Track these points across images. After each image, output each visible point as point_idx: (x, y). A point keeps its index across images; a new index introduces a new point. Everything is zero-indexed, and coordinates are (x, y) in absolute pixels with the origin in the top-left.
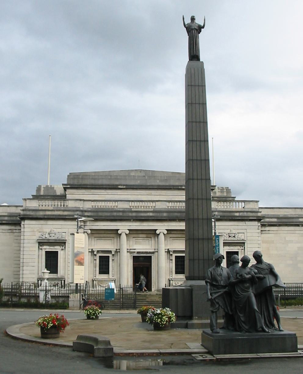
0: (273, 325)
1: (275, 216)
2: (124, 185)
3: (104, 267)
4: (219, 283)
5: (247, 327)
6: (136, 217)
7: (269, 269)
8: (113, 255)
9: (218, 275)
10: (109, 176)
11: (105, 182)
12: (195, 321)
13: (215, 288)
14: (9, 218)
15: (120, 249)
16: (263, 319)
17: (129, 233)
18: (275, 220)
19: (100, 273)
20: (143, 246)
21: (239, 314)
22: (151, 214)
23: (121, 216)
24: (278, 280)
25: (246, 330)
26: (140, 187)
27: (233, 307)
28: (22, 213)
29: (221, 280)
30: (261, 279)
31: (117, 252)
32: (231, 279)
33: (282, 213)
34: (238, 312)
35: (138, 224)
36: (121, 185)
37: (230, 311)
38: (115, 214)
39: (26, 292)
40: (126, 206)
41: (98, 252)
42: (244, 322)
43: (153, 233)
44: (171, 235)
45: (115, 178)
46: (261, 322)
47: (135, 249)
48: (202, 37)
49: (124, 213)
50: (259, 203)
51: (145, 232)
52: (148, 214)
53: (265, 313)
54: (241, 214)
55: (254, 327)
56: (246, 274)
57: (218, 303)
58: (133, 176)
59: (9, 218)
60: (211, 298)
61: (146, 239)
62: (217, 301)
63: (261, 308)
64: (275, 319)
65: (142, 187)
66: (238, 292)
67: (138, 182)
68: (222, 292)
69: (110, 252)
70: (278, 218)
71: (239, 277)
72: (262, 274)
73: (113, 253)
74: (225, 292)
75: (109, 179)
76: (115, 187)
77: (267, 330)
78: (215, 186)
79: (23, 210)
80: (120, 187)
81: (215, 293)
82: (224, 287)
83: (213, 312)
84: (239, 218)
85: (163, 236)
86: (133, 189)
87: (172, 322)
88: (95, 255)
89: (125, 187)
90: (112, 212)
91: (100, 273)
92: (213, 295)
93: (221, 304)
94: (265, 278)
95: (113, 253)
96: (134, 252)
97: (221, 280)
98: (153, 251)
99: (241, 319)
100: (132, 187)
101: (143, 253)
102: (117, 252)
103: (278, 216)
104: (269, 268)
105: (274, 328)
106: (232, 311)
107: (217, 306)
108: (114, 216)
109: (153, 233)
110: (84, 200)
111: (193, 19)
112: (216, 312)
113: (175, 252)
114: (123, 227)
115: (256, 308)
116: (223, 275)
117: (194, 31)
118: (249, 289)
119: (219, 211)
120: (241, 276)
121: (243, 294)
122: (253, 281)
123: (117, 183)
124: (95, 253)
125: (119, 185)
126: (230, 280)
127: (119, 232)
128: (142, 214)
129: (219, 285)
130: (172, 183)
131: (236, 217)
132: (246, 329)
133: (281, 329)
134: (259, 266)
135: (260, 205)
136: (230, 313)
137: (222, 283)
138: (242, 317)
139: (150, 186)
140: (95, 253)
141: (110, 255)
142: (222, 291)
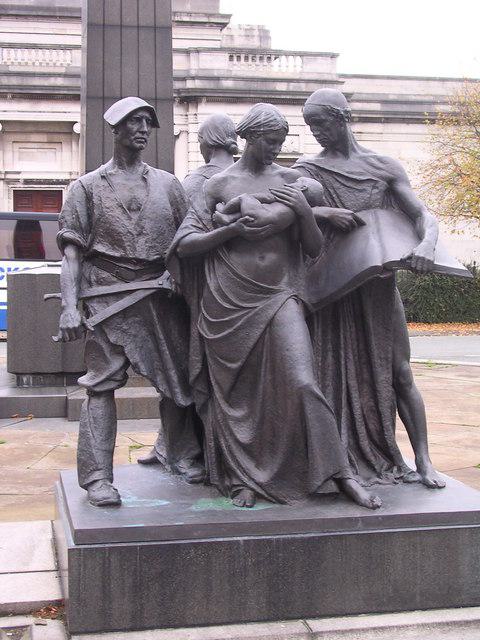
0: (392, 457)
1: (376, 98)
4: (124, 249)
5: (262, 476)
6: (20, 87)
7: (382, 185)
13: (105, 275)
16: (344, 431)
18: (377, 107)
21: (225, 407)
22: (60, 82)
24: (427, 237)
25: (259, 490)
26: (34, 13)
29: (135, 233)
30: (344, 231)
33: (393, 90)
35: (25, 106)
37: (178, 390)
46: (332, 442)
47: (19, 173)
50: (338, 59)
51: (47, 129)
52: (52, 82)
53: (355, 395)
54: (292, 87)
57: (118, 350)
60: (83, 325)
61: (46, 146)
62: (112, 339)
63: (338, 375)
64: (399, 422)
66: (215, 294)
68: (141, 295)
70: (384, 102)
71: (226, 218)
77: (364, 495)
78: (229, 16)
81: (105, 298)
84: (288, 97)
86: (17, 16)
92: (94, 306)
93: (134, 358)
94: (361, 224)
96: (17, 180)
98: (67, 177)
99: (232, 434)
101: (39, 182)
103: (384, 98)
104: (382, 178)
105: (395, 469)
106: (188, 390)
115: (305, 376)
116: (148, 210)
119: (236, 79)
120: (236, 209)
121: (244, 305)
122: (304, 237)
128: (37, 82)
131: (280, 95)
132: (257, 484)
133: (430, 479)
134: (339, 165)
135: (342, 67)
137: (142, 250)
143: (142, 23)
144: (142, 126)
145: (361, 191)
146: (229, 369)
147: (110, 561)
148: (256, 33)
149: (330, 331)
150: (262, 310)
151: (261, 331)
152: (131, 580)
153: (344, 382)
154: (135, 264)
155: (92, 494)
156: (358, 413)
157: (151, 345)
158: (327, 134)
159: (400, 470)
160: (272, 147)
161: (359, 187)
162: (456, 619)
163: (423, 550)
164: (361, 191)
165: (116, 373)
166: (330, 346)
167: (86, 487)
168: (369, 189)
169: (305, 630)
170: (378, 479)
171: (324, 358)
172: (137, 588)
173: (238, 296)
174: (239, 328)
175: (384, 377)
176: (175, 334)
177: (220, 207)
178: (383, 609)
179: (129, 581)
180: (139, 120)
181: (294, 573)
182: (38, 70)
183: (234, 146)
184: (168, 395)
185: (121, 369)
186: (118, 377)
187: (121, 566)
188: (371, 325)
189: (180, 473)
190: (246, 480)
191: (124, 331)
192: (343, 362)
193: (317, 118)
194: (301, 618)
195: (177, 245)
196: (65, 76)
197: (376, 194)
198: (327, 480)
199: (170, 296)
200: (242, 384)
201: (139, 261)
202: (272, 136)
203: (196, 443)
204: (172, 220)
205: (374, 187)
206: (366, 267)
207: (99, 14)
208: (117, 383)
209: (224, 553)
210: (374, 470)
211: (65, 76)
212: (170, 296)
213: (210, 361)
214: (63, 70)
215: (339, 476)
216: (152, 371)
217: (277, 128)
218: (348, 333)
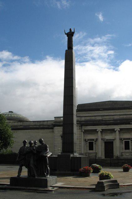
3: (91, 147)
11: (94, 107)
12: (57, 172)
14: (113, 121)
19: (90, 149)
20: (109, 137)
22: (112, 122)
28: (54, 123)
31: (97, 140)
35: (106, 126)
40: (100, 118)
41: (88, 140)
43: (95, 131)
44: (122, 131)
48: (74, 38)
59: (113, 121)
69: (93, 140)
73: (95, 140)
79: (54, 122)
80: (100, 109)
85: (118, 132)
88: (87, 141)
90: (93, 121)
91: (90, 149)
98: (114, 139)
101: (109, 140)
102: (97, 140)
109: (113, 131)
110: (81, 117)
111: (70, 30)
113: (124, 139)
117: (70, 35)
123: (99, 108)
124: (87, 141)
127: (97, 130)
130: (126, 106)
140: (87, 141)
141: (130, 140)
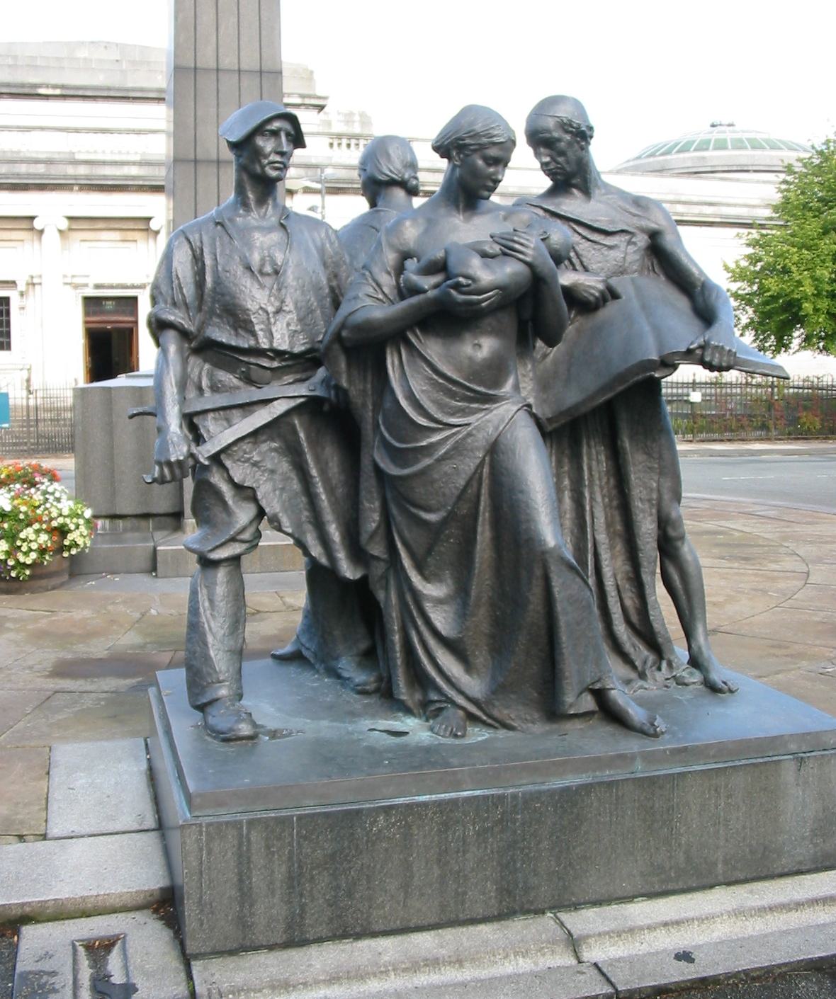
2: (55, 87)
4: (254, 334)
5: (474, 685)
6: (87, 177)
7: (642, 240)
8: (22, 294)
9: (248, 268)
10: (10, 59)
15: (40, 276)
17: (70, 229)
22: (134, 171)
23: (41, 176)
25: (472, 709)
27: (372, 520)
29: (271, 309)
32: (351, 294)
34: (407, 562)
36: (47, 86)
38: (23, 169)
39: (757, 392)
42: (452, 646)
45: (28, 65)
49: (52, 166)
53: (605, 556)
55: (530, 659)
56: (484, 255)
57: (246, 493)
58: (85, 59)
65: (112, 94)
66: (404, 403)
67: (99, 80)
68: (280, 408)
69: (13, 284)
72: (593, 266)
74: (311, 407)
75: (10, 66)
76: (26, 91)
78: (325, 98)
80: (42, 91)
82: (305, 362)
83: (207, 564)
87: (74, 552)
89: (58, 92)
92: (209, 425)
93: (273, 505)
95: (21, 286)
96: (86, 285)
97: (271, 309)
100: (80, 93)
101: (111, 287)
104: (643, 230)
106: (358, 554)
107: (244, 514)
108: (18, 175)
112: (235, 560)
114: (51, 209)
118: (497, 383)
119: (335, 166)
122: (534, 310)
125: (40, 86)
126: (344, 310)
128: (108, 171)
129: (257, 352)
136: (349, 571)
138: (439, 602)
139: (134, 90)
142: (285, 395)
143: (244, 66)
144: (280, 144)
145: (611, 248)
146: (425, 523)
147: (249, 840)
148: (357, 118)
149: (566, 460)
150: (478, 428)
151: (478, 461)
152: (284, 868)
153: (589, 537)
154: (272, 359)
155: (211, 720)
156: (609, 584)
157: (296, 485)
158: (560, 159)
159: (670, 664)
160: (492, 170)
161: (609, 241)
162: (782, 899)
163: (729, 796)
164: (611, 248)
165: (243, 530)
166: (566, 482)
167: (201, 708)
168: (623, 246)
169: (560, 933)
170: (641, 683)
171: (560, 500)
172: (293, 881)
173: (441, 406)
174: (439, 460)
175: (647, 527)
176: (334, 467)
177: (411, 264)
178: (670, 887)
179: (280, 872)
180: (275, 133)
181: (539, 843)
182: (108, 158)
183: (414, 182)
184: (324, 561)
185: (251, 522)
186: (246, 536)
187: (268, 847)
188: (628, 449)
189: (339, 677)
190: (451, 693)
191: (255, 464)
192: (588, 508)
193: (547, 135)
194: (551, 908)
195: (343, 326)
196: (140, 164)
197: (628, 253)
198: (581, 693)
199: (326, 407)
200: (450, 545)
201: (279, 354)
202: (493, 152)
203: (221, 509)
204: (327, 291)
205: (629, 243)
206: (633, 361)
207: (190, 55)
208: (244, 546)
209: (432, 819)
210: (634, 667)
211: (140, 164)
212: (326, 407)
213: (394, 510)
214: (137, 158)
215: (597, 686)
216: (298, 525)
217: (502, 140)
218: (595, 461)
